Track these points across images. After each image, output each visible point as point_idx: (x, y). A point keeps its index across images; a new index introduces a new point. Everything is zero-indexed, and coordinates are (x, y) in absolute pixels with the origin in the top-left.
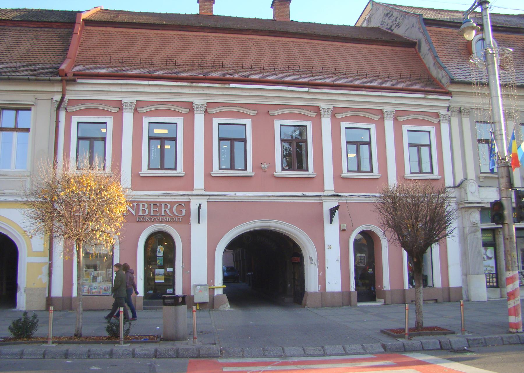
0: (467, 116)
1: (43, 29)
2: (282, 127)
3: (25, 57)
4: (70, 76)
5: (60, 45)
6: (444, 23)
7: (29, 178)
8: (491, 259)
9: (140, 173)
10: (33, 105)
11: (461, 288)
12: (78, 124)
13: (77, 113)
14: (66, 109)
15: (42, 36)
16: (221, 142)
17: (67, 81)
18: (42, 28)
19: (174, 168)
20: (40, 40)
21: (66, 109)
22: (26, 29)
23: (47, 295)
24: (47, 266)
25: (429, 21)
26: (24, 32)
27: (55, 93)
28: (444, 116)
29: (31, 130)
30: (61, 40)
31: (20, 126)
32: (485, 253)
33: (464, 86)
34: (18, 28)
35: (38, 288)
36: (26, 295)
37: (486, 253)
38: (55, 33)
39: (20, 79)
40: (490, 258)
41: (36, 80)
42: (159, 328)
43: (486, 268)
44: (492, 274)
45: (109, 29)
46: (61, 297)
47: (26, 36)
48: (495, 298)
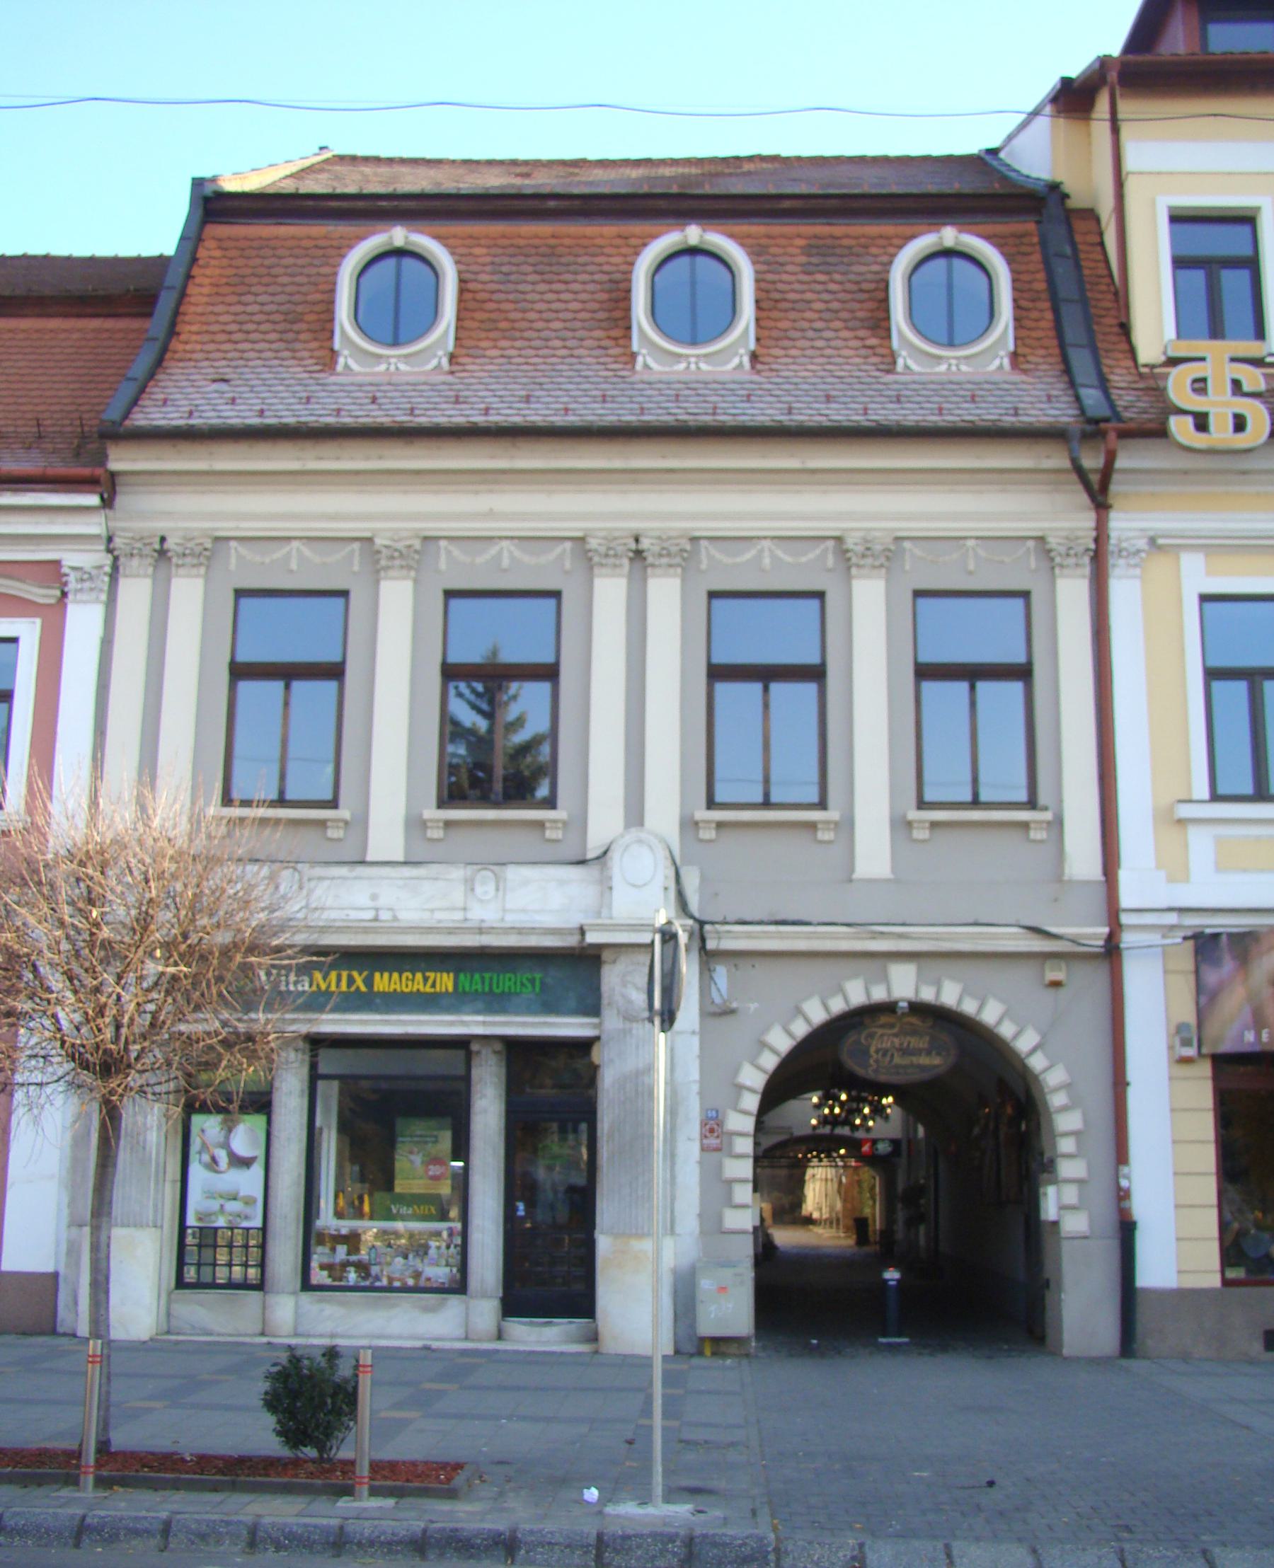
0: (194, 571)
2: (1208, 606)
6: (298, 203)
8: (248, 1168)
11: (55, 1275)
12: (709, 604)
25: (236, 203)
28: (85, 576)
32: (222, 1139)
33: (174, 446)
37: (227, 1138)
40: (244, 1163)
43: (221, 1201)
44: (248, 1229)
48: (230, 1335)
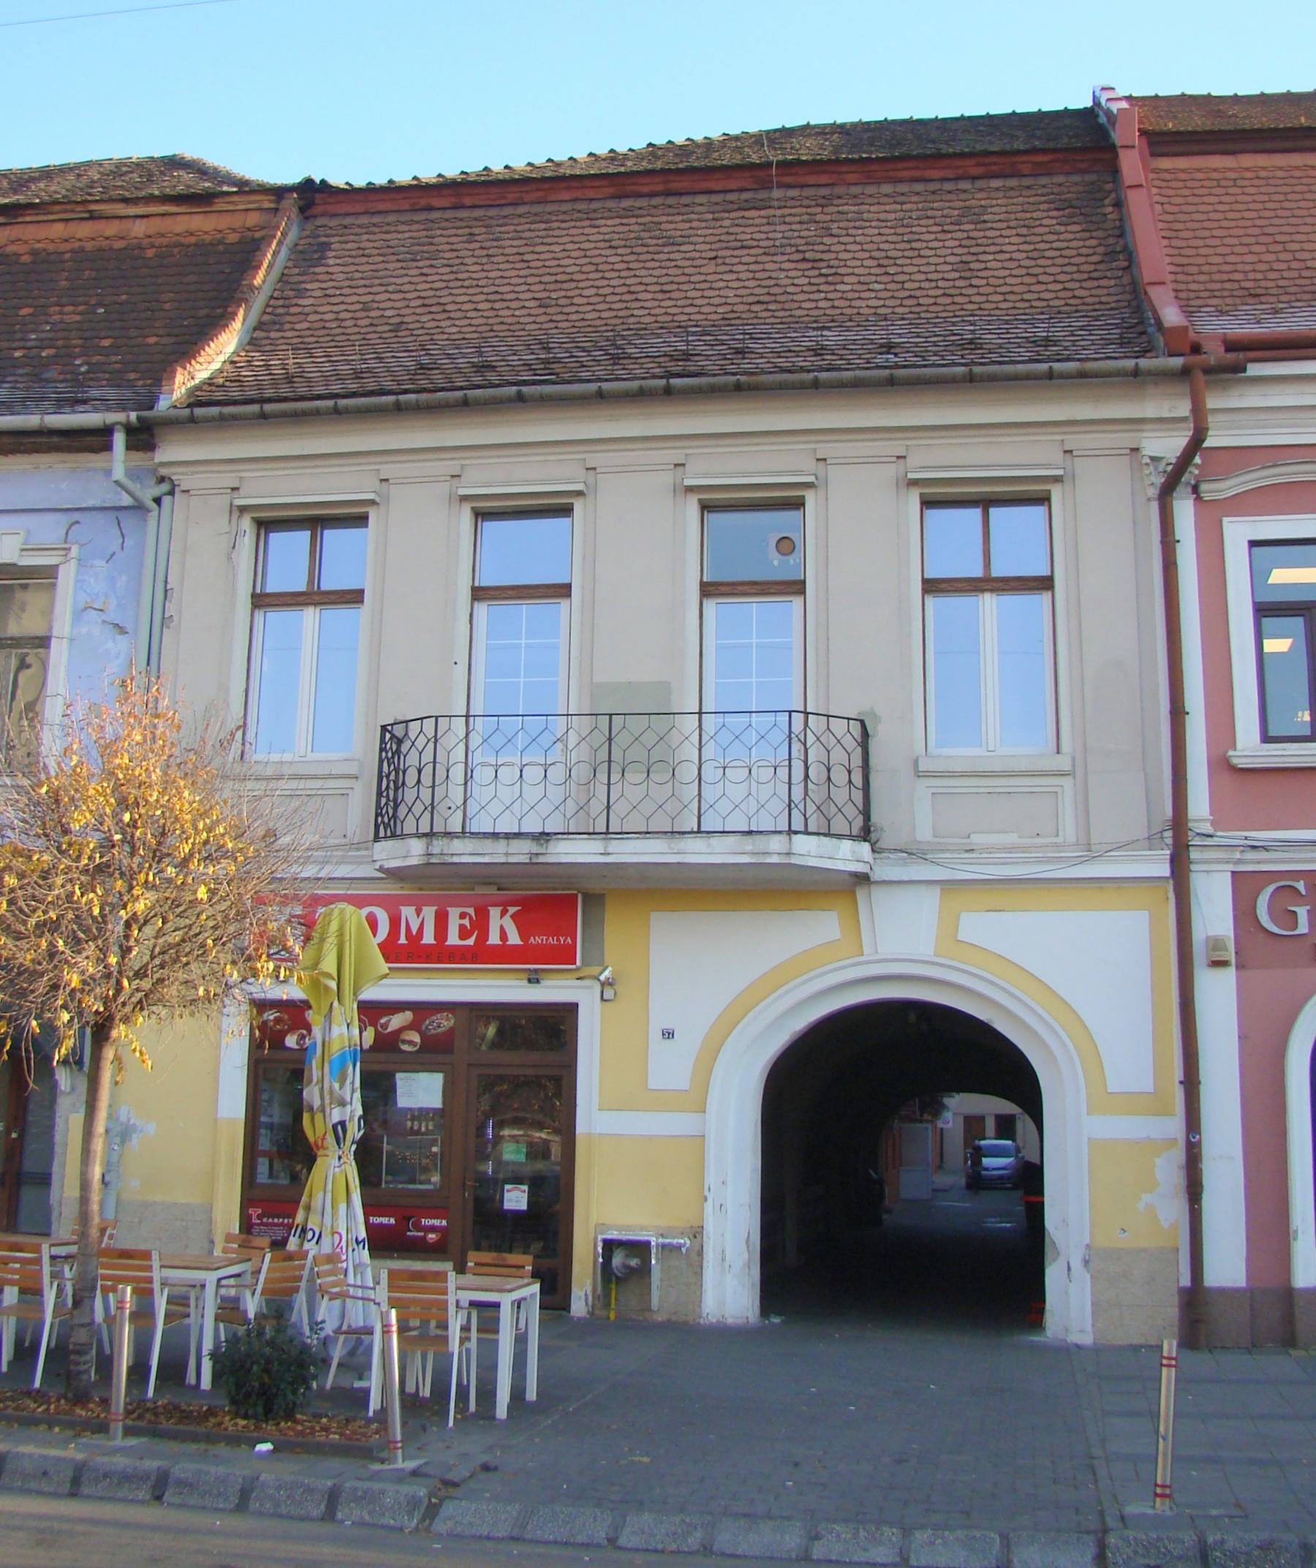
1: (979, 184)
3: (439, 304)
4: (1215, 353)
5: (1078, 236)
7: (1067, 782)
9: (1231, 753)
10: (1057, 479)
13: (1243, 504)
14: (1195, 489)
15: (990, 210)
16: (1265, 621)
17: (1208, 371)
18: (974, 178)
19: (1272, 733)
20: (989, 225)
21: (1195, 489)
22: (919, 187)
23: (1186, 1281)
24: (1179, 1155)
26: (913, 199)
27: (1146, 427)
29: (575, 590)
30: (1075, 220)
31: (997, 572)
34: (887, 188)
35: (1144, 1250)
36: (1092, 1277)
38: (1033, 192)
39: (1016, 377)
41: (1082, 375)
42: (435, 1546)
45: (1247, 160)
46: (1235, 1291)
47: (930, 213)
